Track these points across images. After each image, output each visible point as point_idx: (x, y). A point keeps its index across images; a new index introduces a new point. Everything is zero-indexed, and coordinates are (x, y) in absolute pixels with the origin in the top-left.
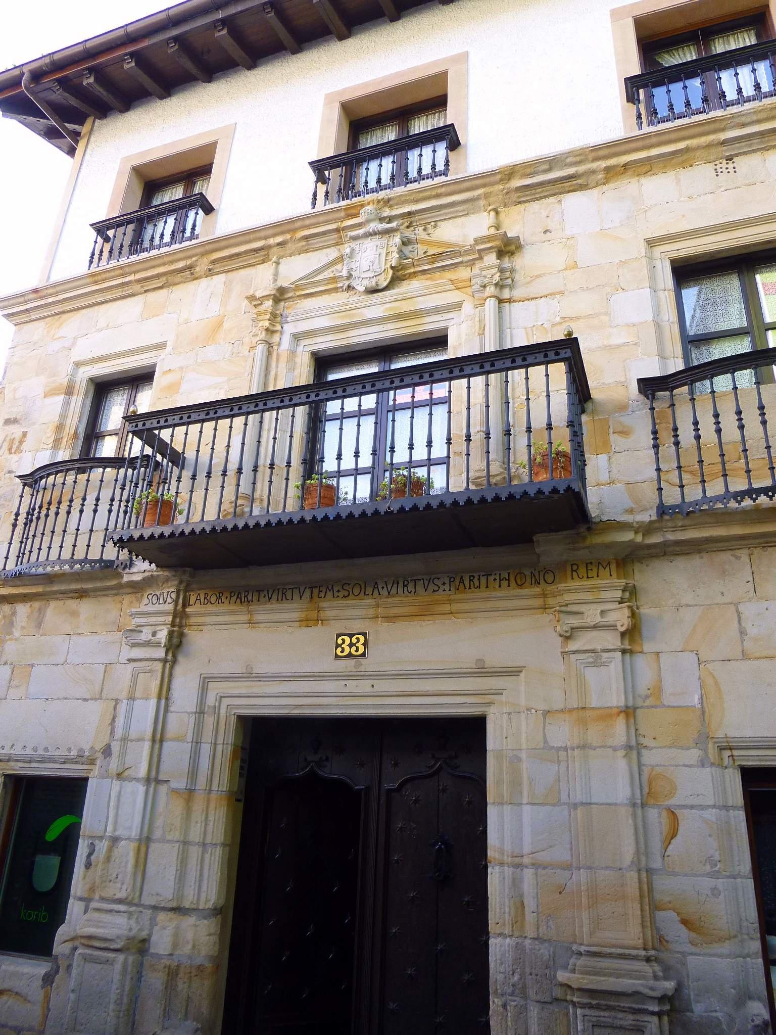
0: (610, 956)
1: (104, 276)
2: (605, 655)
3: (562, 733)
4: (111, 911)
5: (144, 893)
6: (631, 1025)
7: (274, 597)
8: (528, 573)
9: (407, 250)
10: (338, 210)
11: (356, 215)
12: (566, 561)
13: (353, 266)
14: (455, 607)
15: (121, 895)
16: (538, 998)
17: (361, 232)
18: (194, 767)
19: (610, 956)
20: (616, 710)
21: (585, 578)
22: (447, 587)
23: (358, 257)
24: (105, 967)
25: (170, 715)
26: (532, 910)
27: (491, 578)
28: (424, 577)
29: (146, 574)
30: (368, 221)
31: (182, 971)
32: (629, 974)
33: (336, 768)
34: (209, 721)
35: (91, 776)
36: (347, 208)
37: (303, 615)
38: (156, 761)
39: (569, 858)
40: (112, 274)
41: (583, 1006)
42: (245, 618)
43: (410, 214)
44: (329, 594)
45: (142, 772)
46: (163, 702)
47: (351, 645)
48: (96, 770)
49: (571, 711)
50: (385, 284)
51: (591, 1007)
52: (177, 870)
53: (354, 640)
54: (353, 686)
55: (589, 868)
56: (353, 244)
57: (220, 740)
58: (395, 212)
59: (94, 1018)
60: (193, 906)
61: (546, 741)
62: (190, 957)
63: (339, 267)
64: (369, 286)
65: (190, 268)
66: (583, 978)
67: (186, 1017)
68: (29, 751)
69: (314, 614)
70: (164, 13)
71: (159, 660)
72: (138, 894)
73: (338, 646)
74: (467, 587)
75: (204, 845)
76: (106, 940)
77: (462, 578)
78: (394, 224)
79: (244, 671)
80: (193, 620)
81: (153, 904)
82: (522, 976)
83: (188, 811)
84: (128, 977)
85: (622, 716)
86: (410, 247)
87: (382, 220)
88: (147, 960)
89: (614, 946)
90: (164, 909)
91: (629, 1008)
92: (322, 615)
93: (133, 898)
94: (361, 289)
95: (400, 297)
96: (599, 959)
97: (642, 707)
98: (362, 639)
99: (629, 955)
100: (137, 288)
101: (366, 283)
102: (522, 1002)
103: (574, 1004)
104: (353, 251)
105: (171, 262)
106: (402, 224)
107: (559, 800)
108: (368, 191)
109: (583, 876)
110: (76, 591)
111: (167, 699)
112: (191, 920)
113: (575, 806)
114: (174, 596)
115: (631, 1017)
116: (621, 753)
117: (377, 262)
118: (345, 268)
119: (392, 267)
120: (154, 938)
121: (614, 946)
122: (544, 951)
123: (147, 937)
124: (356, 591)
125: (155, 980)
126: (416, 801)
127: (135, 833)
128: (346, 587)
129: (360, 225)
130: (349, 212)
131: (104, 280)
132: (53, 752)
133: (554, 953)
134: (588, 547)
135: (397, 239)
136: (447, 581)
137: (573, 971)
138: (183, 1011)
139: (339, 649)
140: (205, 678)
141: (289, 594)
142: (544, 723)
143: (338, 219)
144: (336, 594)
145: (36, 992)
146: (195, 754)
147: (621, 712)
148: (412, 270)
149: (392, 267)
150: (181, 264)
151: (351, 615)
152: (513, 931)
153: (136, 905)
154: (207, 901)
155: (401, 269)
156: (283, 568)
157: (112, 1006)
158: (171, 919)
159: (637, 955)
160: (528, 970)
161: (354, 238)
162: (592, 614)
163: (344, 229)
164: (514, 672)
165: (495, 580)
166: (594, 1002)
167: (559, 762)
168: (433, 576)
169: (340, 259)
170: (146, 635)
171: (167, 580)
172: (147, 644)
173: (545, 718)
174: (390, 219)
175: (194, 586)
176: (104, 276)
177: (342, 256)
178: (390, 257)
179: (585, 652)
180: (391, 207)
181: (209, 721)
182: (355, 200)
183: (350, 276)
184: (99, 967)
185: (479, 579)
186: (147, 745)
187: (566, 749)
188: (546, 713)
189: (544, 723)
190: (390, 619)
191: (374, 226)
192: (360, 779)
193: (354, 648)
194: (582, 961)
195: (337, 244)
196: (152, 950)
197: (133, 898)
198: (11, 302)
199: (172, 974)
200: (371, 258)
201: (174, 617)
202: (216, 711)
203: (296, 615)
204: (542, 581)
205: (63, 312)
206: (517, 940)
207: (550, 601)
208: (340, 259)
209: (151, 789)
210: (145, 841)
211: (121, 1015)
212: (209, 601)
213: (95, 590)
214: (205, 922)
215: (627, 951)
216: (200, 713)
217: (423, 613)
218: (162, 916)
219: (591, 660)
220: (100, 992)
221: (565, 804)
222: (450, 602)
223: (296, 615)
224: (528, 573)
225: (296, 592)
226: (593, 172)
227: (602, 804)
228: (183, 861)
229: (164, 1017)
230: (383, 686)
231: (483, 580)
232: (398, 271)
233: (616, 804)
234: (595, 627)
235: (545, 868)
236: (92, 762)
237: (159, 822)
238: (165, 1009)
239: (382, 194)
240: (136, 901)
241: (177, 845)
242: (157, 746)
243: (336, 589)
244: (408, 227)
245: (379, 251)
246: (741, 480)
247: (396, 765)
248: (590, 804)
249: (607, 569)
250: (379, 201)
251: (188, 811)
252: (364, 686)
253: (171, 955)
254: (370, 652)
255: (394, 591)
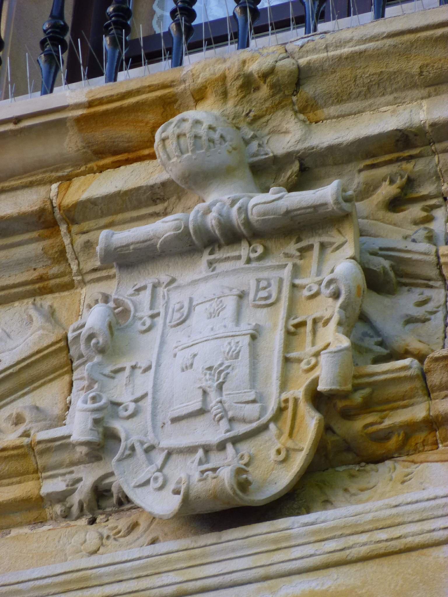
9: (390, 313)
10: (50, 124)
13: (122, 391)
17: (162, 227)
23: (146, 350)
30: (199, 178)
36: (93, 117)
43: (404, 142)
50: (283, 478)
56: (121, 288)
58: (329, 135)
63: (48, 396)
64: (199, 488)
70: (430, 459)
78: (325, 193)
86: (407, 302)
87: (263, 171)
94: (163, 504)
95: (362, 544)
101: (186, 472)
104: (120, 317)
106: (367, 191)
108: (193, 36)
117: (241, 370)
118: (80, 403)
119: (318, 399)
129: (155, 198)
130: (102, 135)
135: (342, 265)
143: (42, 166)
148: (418, 412)
149: (318, 399)
155: (367, 407)
161: (130, 260)
163: (80, 214)
169: (56, 360)
174: (306, 169)
177: (64, 345)
178: (305, 349)
180: (309, 111)
182: (130, 78)
183: (104, 443)
191: (221, 202)
195: (41, 287)
200: (210, 353)
208: (56, 360)
232: (348, 415)
239: (266, 52)
244: (395, 204)
245: (253, 317)
246: (420, 399)
250: (248, 84)
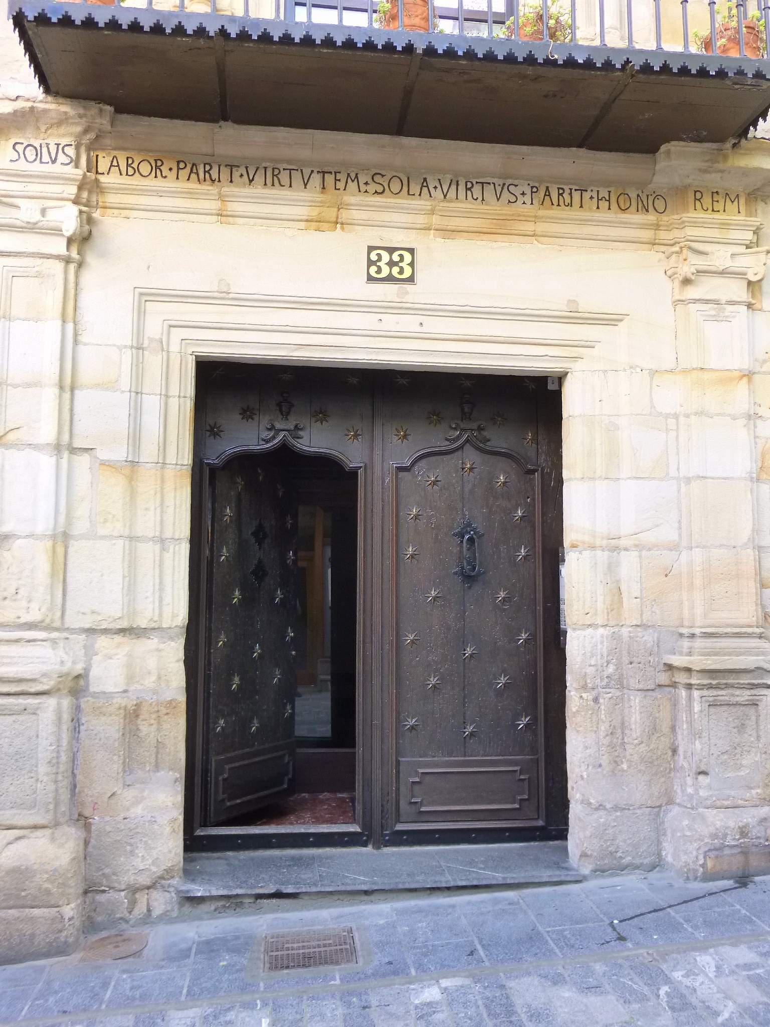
0: (726, 635)
2: (730, 308)
3: (671, 396)
4: (17, 641)
5: (68, 613)
6: (748, 700)
7: (259, 179)
8: (633, 195)
12: (686, 188)
14: (541, 227)
15: (34, 616)
16: (641, 686)
18: (135, 429)
19: (726, 635)
20: (737, 374)
21: (710, 211)
22: (527, 199)
24: (21, 718)
25: (81, 348)
26: (636, 595)
27: (586, 195)
28: (495, 180)
29: (20, 105)
31: (145, 709)
32: (748, 652)
33: (317, 439)
34: (154, 362)
37: (315, 212)
38: (68, 418)
39: (676, 538)
41: (701, 687)
42: (214, 205)
44: (352, 186)
45: (47, 432)
46: (70, 326)
47: (391, 264)
49: (685, 371)
51: (710, 687)
52: (124, 577)
53: (396, 257)
54: (391, 322)
55: (704, 547)
57: (174, 390)
59: (12, 788)
60: (153, 625)
61: (653, 407)
62: (155, 692)
66: (707, 660)
67: (157, 767)
69: (331, 213)
71: (58, 257)
72: (59, 614)
73: (370, 263)
74: (555, 202)
75: (162, 541)
76: (21, 681)
77: (547, 188)
79: (216, 289)
80: (111, 199)
81: (87, 626)
82: (618, 666)
83: (132, 493)
84: (65, 727)
85: (745, 380)
88: (86, 703)
89: (728, 626)
90: (106, 631)
91: (749, 684)
92: (344, 215)
93: (52, 621)
96: (715, 640)
97: (759, 373)
98: (408, 257)
99: (745, 633)
102: (618, 693)
103: (689, 687)
107: (668, 474)
109: (698, 555)
111: (75, 323)
112: (153, 643)
113: (688, 480)
114: (71, 151)
115: (748, 692)
116: (743, 421)
120: (93, 674)
121: (728, 626)
122: (648, 638)
123: (82, 672)
124: (396, 186)
125: (105, 728)
126: (435, 483)
127: (44, 523)
128: (378, 178)
133: (658, 639)
134: (722, 171)
136: (528, 191)
137: (690, 654)
138: (153, 760)
139: (373, 269)
140: (141, 294)
141: (284, 177)
142: (651, 385)
144: (363, 187)
146: (136, 409)
147: (744, 376)
151: (391, 220)
152: (608, 620)
153: (57, 629)
154: (174, 616)
156: (282, 133)
157: (43, 769)
158: (119, 646)
159: (753, 633)
160: (625, 660)
162: (720, 257)
164: (611, 320)
165: (592, 198)
166: (714, 682)
167: (667, 430)
168: (508, 182)
170: (28, 212)
171: (62, 121)
172: (31, 228)
173: (652, 379)
175: (107, 141)
179: (707, 302)
181: (154, 362)
184: (9, 719)
185: (571, 194)
186: (50, 394)
187: (676, 416)
188: (653, 373)
189: (651, 385)
190: (448, 233)
192: (352, 452)
193: (395, 270)
194: (699, 643)
196: (93, 688)
197: (52, 621)
199: (133, 715)
201: (80, 188)
202: (162, 346)
203: (302, 211)
204: (651, 208)
206: (612, 630)
207: (663, 235)
209: (64, 462)
210: (62, 538)
211: (60, 777)
212: (137, 170)
214: (173, 644)
215: (743, 630)
216: (138, 349)
217: (497, 230)
218: (103, 642)
219: (713, 313)
220: (17, 753)
221: (674, 478)
222: (536, 219)
223: (302, 211)
224: (633, 195)
225: (296, 175)
227: (719, 478)
228: (132, 563)
229: (125, 771)
230: (435, 325)
231: (576, 196)
233: (732, 478)
234: (723, 273)
235: (650, 550)
237: (82, 511)
238: (124, 762)
240: (57, 624)
241: (120, 542)
242: (67, 395)
243: (362, 180)
247: (405, 436)
248: (705, 478)
249: (736, 203)
251: (132, 493)
252: (409, 323)
253: (125, 691)
254: (418, 277)
255: (452, 194)
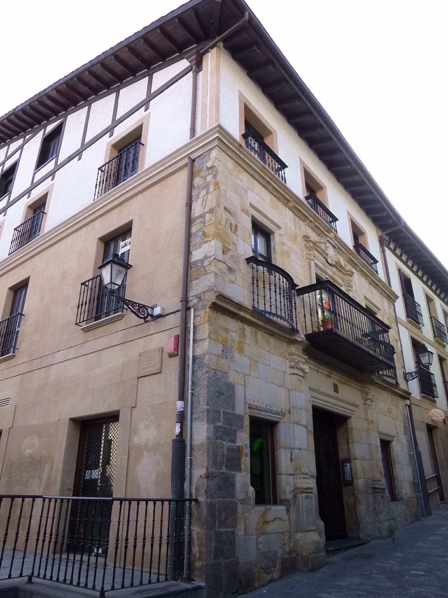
1: (266, 172)
11: (329, 233)
35: (353, 416)
40: (269, 175)
48: (286, 419)
65: (289, 201)
68: (264, 406)
100: (270, 188)
105: (286, 193)
110: (270, 331)
131: (264, 173)
132: (273, 408)
145: (285, 516)
150: (288, 198)
176: (266, 172)
198: (226, 136)
205: (240, 165)
213: (282, 336)
226: (359, 267)
236: (284, 415)
252: (336, 402)
